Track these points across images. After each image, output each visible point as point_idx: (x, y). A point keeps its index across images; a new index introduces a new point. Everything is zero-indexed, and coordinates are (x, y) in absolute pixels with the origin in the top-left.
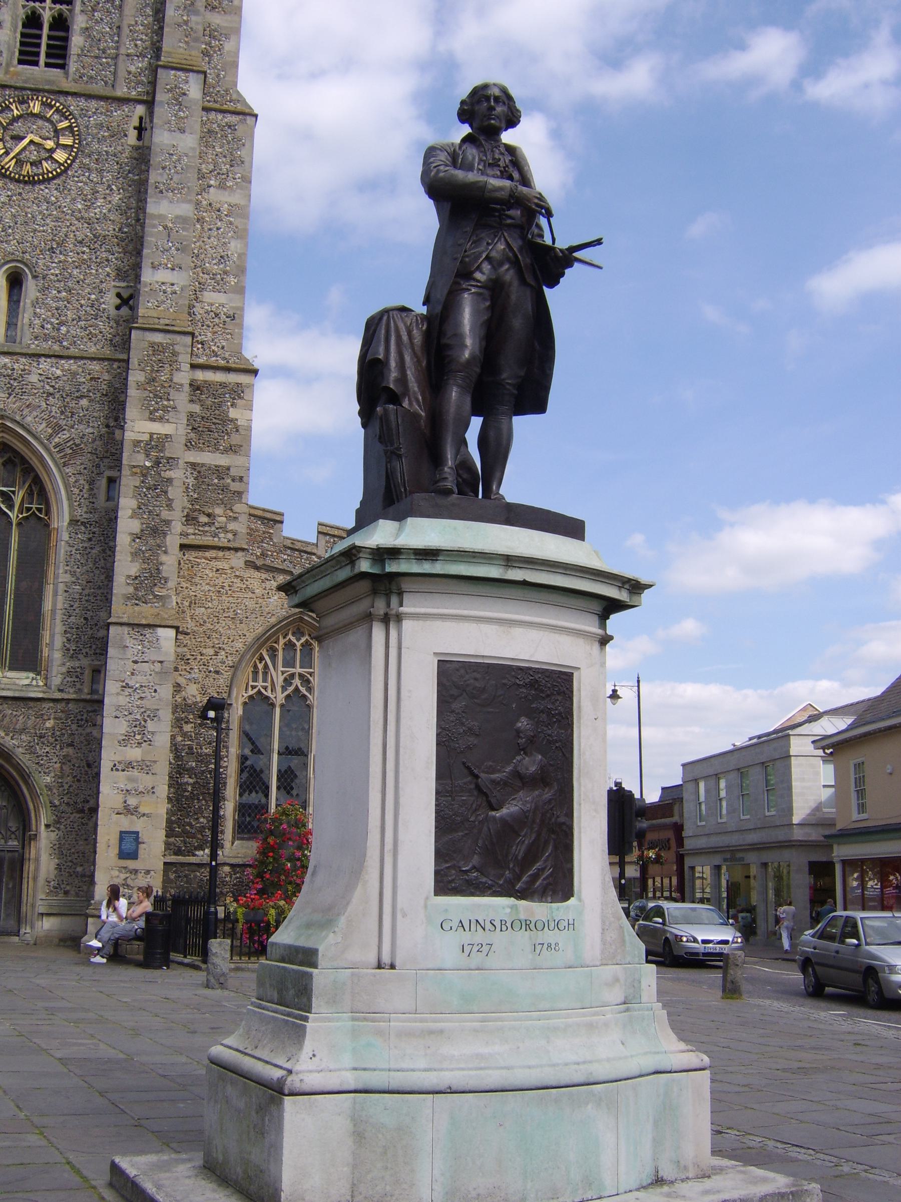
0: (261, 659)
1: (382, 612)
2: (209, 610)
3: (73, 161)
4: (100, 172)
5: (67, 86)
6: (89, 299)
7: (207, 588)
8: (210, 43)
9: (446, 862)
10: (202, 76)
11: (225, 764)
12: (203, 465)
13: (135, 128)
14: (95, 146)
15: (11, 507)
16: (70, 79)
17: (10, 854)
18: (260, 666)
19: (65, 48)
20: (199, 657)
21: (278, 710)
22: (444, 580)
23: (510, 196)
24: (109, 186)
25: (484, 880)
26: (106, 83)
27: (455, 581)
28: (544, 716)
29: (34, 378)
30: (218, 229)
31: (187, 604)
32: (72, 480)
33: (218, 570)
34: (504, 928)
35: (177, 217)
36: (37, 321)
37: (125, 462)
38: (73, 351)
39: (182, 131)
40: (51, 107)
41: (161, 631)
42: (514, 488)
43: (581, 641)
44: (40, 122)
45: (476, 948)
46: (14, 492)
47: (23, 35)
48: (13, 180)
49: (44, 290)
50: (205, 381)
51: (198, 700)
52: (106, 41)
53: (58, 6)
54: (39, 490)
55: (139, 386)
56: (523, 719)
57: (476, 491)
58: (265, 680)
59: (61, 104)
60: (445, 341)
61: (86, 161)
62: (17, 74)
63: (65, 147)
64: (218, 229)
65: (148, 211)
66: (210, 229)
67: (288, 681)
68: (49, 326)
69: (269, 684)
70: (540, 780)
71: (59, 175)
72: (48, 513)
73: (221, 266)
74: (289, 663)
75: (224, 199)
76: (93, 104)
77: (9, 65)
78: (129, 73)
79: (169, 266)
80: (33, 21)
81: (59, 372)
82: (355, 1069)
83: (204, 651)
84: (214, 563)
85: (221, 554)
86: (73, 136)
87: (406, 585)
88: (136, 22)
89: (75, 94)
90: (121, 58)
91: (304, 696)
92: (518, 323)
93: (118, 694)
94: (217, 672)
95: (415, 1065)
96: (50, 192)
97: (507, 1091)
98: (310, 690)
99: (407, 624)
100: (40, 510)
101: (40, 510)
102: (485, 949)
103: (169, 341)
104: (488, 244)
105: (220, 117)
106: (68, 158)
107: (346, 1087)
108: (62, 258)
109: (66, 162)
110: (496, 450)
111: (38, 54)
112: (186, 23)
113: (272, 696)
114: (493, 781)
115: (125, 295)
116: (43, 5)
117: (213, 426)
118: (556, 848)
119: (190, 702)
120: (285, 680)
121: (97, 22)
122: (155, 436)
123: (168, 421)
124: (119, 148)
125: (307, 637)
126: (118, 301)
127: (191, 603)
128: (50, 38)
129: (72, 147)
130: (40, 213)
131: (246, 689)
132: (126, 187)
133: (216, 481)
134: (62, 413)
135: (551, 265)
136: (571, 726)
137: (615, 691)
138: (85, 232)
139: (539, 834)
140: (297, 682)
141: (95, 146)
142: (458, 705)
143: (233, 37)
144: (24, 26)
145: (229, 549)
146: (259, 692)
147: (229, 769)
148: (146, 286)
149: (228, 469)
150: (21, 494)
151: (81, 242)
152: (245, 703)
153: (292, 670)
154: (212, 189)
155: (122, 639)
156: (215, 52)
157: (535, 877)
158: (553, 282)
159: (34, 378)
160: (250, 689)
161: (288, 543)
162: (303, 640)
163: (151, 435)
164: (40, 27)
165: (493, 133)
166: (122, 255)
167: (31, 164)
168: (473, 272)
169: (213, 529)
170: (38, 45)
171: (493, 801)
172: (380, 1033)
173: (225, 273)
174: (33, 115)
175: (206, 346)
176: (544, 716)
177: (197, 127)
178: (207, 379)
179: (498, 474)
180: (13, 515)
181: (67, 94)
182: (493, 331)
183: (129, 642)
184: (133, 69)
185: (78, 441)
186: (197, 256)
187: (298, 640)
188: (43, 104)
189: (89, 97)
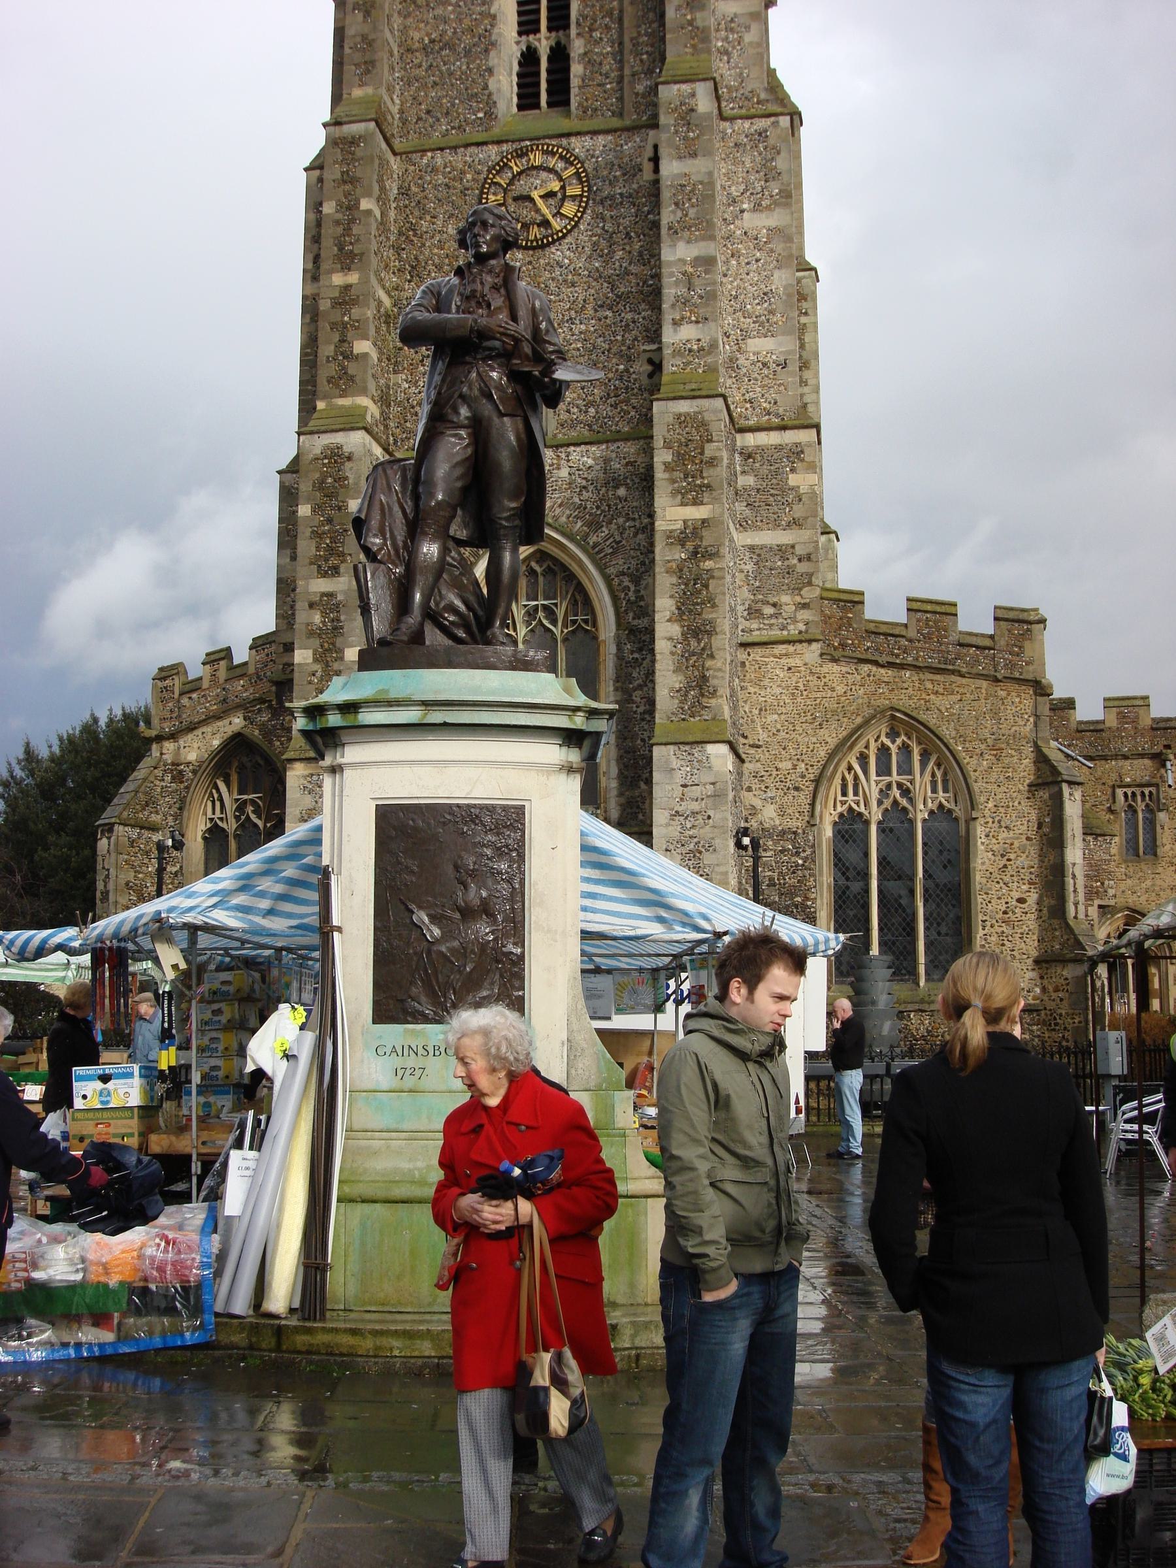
0: (850, 768)
2: (783, 717)
6: (617, 370)
7: (778, 691)
8: (727, 38)
10: (710, 84)
11: (813, 896)
12: (762, 547)
13: (650, 160)
15: (554, 622)
16: (573, 116)
18: (850, 778)
20: (775, 773)
21: (873, 829)
22: (382, 729)
24: (628, 234)
27: (393, 730)
30: (757, 261)
31: (757, 712)
33: (790, 669)
34: (437, 1053)
35: (697, 259)
37: (657, 558)
39: (694, 155)
41: (710, 748)
44: (544, 175)
45: (408, 1072)
46: (556, 605)
50: (758, 447)
51: (777, 822)
55: (668, 467)
58: (856, 794)
59: (564, 149)
63: (573, 198)
64: (757, 261)
65: (663, 258)
66: (748, 263)
67: (884, 793)
68: (576, 410)
69: (861, 798)
72: (595, 624)
73: (766, 305)
74: (884, 769)
75: (760, 224)
78: (637, 94)
79: (693, 318)
80: (529, 58)
83: (780, 766)
84: (783, 661)
85: (791, 648)
86: (581, 183)
88: (639, 33)
89: (578, 134)
91: (905, 810)
93: (668, 825)
94: (797, 789)
98: (911, 801)
100: (586, 621)
101: (586, 621)
102: (418, 1073)
103: (697, 409)
105: (747, 124)
106: (578, 211)
108: (583, 327)
109: (576, 215)
112: (690, 23)
113: (866, 813)
116: (538, 36)
117: (772, 499)
119: (767, 825)
120: (881, 791)
122: (690, 523)
123: (702, 503)
125: (903, 737)
126: (650, 368)
127: (761, 710)
129: (581, 196)
130: (553, 279)
131: (835, 806)
132: (647, 231)
133: (779, 563)
140: (896, 792)
145: (801, 642)
146: (850, 809)
147: (818, 902)
149: (793, 547)
151: (601, 306)
152: (835, 823)
153: (888, 779)
154: (746, 215)
155: (667, 762)
156: (734, 48)
160: (839, 804)
161: (872, 627)
162: (899, 741)
163: (685, 522)
166: (649, 312)
167: (539, 225)
169: (781, 620)
173: (772, 312)
174: (534, 168)
175: (755, 405)
178: (759, 443)
180: (557, 631)
181: (568, 135)
183: (675, 763)
185: (618, 538)
186: (736, 297)
187: (893, 742)
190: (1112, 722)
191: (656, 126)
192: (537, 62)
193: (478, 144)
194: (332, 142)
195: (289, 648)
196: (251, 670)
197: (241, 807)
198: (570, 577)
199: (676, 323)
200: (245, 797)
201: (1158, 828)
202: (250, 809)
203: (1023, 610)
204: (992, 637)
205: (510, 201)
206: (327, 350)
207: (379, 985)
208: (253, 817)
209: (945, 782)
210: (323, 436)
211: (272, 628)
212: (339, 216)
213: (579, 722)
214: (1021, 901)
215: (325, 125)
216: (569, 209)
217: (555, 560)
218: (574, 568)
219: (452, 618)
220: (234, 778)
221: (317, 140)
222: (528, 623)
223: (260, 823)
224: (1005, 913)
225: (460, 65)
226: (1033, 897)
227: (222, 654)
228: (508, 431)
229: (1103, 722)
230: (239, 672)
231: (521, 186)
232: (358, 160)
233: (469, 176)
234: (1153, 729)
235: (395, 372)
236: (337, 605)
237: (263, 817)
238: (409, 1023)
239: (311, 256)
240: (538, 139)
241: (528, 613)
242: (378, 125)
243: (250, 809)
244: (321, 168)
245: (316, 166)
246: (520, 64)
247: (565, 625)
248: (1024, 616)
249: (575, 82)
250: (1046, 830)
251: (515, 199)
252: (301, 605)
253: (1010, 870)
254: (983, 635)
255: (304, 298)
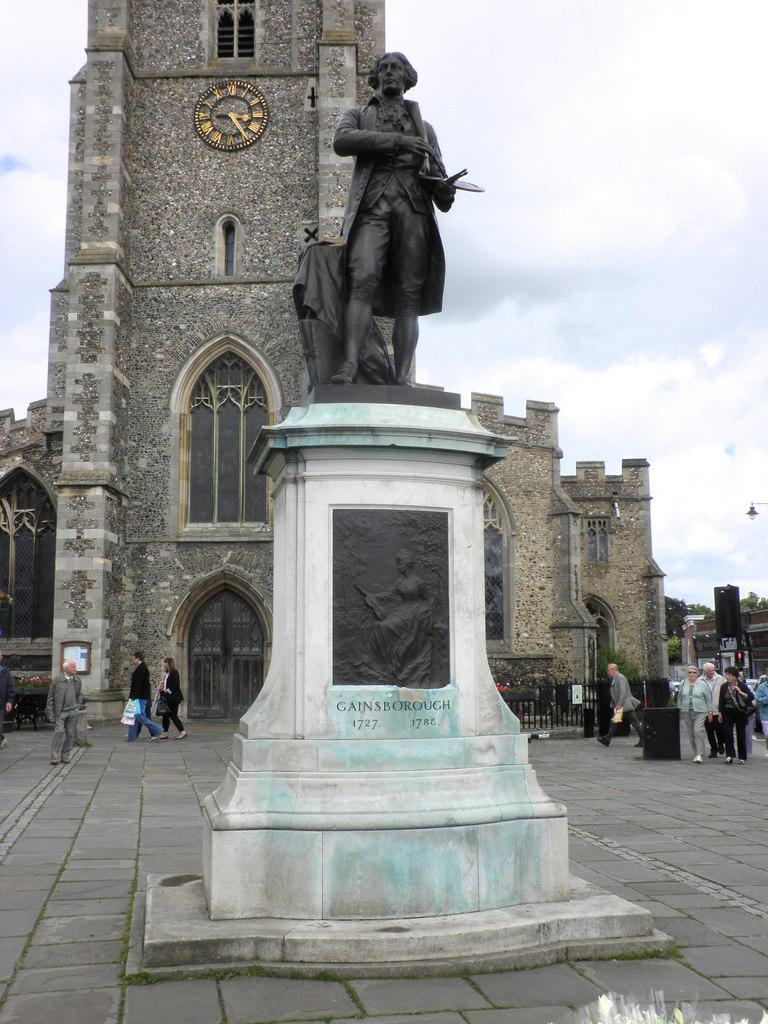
1: (292, 477)
3: (264, 130)
4: (285, 136)
5: (255, 69)
9: (342, 659)
10: (354, 48)
13: (309, 98)
14: (280, 116)
15: (239, 400)
17: (253, 658)
19: (252, 39)
23: (395, 145)
24: (293, 146)
25: (372, 672)
26: (285, 64)
28: (421, 548)
29: (248, 301)
32: (281, 376)
34: (387, 708)
36: (247, 257)
38: (276, 277)
39: (342, 95)
40: (245, 88)
42: (424, 372)
43: (453, 489)
44: (237, 102)
46: (239, 388)
47: (220, 33)
48: (221, 150)
49: (250, 233)
52: (282, 29)
53: (244, 5)
54: (257, 385)
56: (403, 550)
57: (387, 376)
60: (351, 265)
61: (274, 128)
62: (218, 65)
63: (258, 119)
70: (420, 595)
71: (255, 142)
76: (276, 82)
77: (211, 58)
78: (301, 53)
80: (226, 20)
81: (266, 295)
82: (269, 812)
87: (307, 455)
90: (294, 41)
92: (413, 244)
95: (310, 808)
96: (248, 156)
97: (295, 830)
99: (309, 485)
101: (260, 400)
102: (372, 724)
104: (384, 185)
107: (261, 825)
110: (405, 345)
111: (232, 47)
114: (378, 599)
115: (312, 231)
118: (433, 646)
121: (273, 14)
124: (298, 115)
128: (240, 32)
134: (271, 325)
135: (443, 192)
136: (445, 553)
137: (752, 509)
138: (277, 184)
139: (417, 638)
141: (280, 116)
142: (348, 543)
143: (379, 11)
144: (220, 25)
148: (323, 221)
150: (246, 388)
151: (275, 193)
157: (415, 669)
158: (445, 206)
159: (248, 301)
164: (232, 24)
165: (393, 94)
167: (234, 136)
168: (371, 209)
170: (232, 40)
171: (378, 613)
172: (291, 786)
176: (421, 548)
177: (353, 90)
179: (406, 363)
180: (241, 405)
181: (255, 76)
182: (392, 253)
184: (303, 49)
188: (238, 87)
189: (272, 76)
190: (582, 477)
191: (317, 76)
192: (231, 24)
193: (192, 77)
194: (93, 64)
195: (59, 410)
196: (28, 425)
197: (19, 518)
198: (249, 370)
199: (328, 206)
200: (22, 511)
201: (609, 544)
202: (25, 519)
203: (544, 403)
204: (524, 420)
205: (214, 118)
206: (89, 209)
207: (338, 654)
208: (28, 525)
209: (493, 510)
210: (86, 267)
211: (44, 396)
212: (97, 117)
213: (479, 448)
214: (542, 588)
215: (87, 51)
216: (254, 127)
217: (240, 358)
218: (253, 364)
219: (374, 367)
220: (14, 498)
221: (79, 60)
222: (220, 400)
223: (33, 530)
224: (532, 596)
225: (178, 19)
226: (550, 586)
227: (8, 413)
228: (413, 225)
229: (576, 477)
230: (19, 426)
231: (221, 109)
232: (110, 78)
233: (186, 99)
234: (608, 482)
235: (134, 228)
236: (95, 382)
237: (35, 525)
238: (362, 684)
239: (75, 144)
240: (234, 77)
241: (221, 394)
242: (125, 55)
243: (25, 519)
244: (83, 82)
245: (79, 81)
246: (220, 24)
247: (246, 402)
248: (544, 407)
249: (258, 40)
250: (558, 543)
251: (218, 117)
252: (70, 381)
253: (535, 569)
254: (520, 419)
255: (70, 172)
